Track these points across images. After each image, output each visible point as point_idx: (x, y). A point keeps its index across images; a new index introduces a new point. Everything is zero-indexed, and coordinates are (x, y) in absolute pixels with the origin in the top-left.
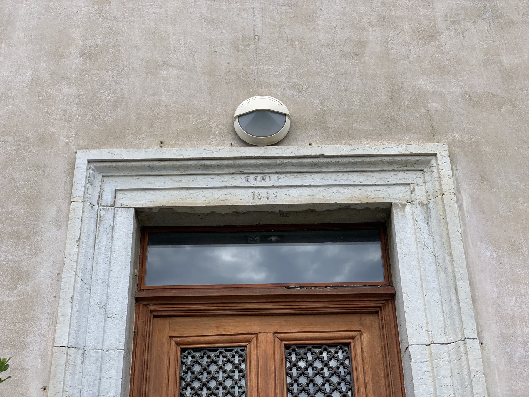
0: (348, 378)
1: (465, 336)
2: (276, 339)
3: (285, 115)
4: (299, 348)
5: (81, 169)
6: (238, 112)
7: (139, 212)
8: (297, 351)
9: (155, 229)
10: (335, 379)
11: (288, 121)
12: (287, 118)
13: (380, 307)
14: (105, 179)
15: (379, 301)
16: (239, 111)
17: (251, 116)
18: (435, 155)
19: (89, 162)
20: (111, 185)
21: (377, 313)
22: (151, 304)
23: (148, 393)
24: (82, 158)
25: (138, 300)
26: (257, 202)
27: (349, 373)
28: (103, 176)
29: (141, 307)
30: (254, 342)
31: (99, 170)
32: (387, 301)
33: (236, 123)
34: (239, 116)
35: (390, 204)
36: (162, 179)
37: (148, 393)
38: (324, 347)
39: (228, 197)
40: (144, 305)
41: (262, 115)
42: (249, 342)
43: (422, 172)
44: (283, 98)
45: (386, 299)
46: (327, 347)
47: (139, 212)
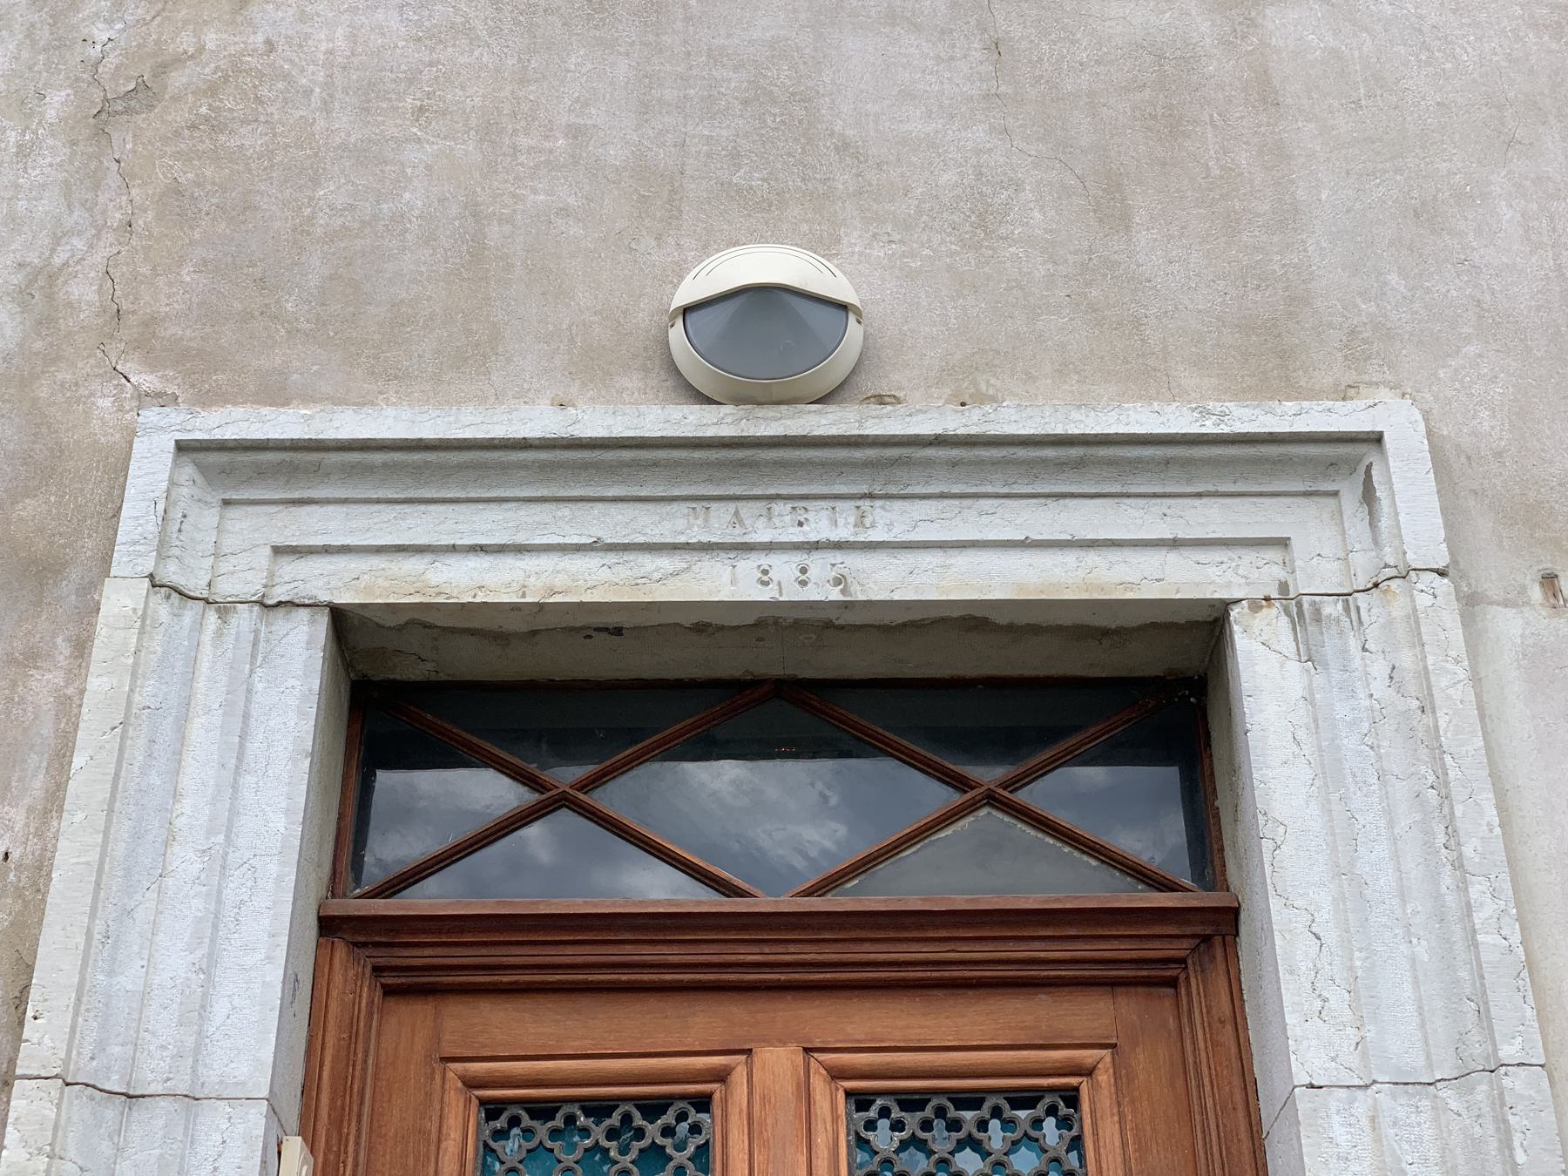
1: (1375, 1077)
3: (843, 307)
4: (1017, 1104)
5: (151, 465)
8: (952, 1113)
9: (401, 698)
11: (854, 331)
12: (852, 318)
13: (1183, 961)
15: (1182, 945)
16: (691, 290)
17: (731, 306)
18: (1377, 439)
19: (182, 448)
21: (1172, 983)
22: (381, 949)
23: (1111, 463)
25: (328, 926)
30: (739, 1077)
32: (1206, 939)
33: (677, 334)
34: (686, 311)
35: (1226, 605)
37: (1111, 463)
38: (1048, 1100)
40: (355, 944)
42: (1089, 1072)
43: (1331, 501)
45: (1198, 930)
46: (949, 1104)
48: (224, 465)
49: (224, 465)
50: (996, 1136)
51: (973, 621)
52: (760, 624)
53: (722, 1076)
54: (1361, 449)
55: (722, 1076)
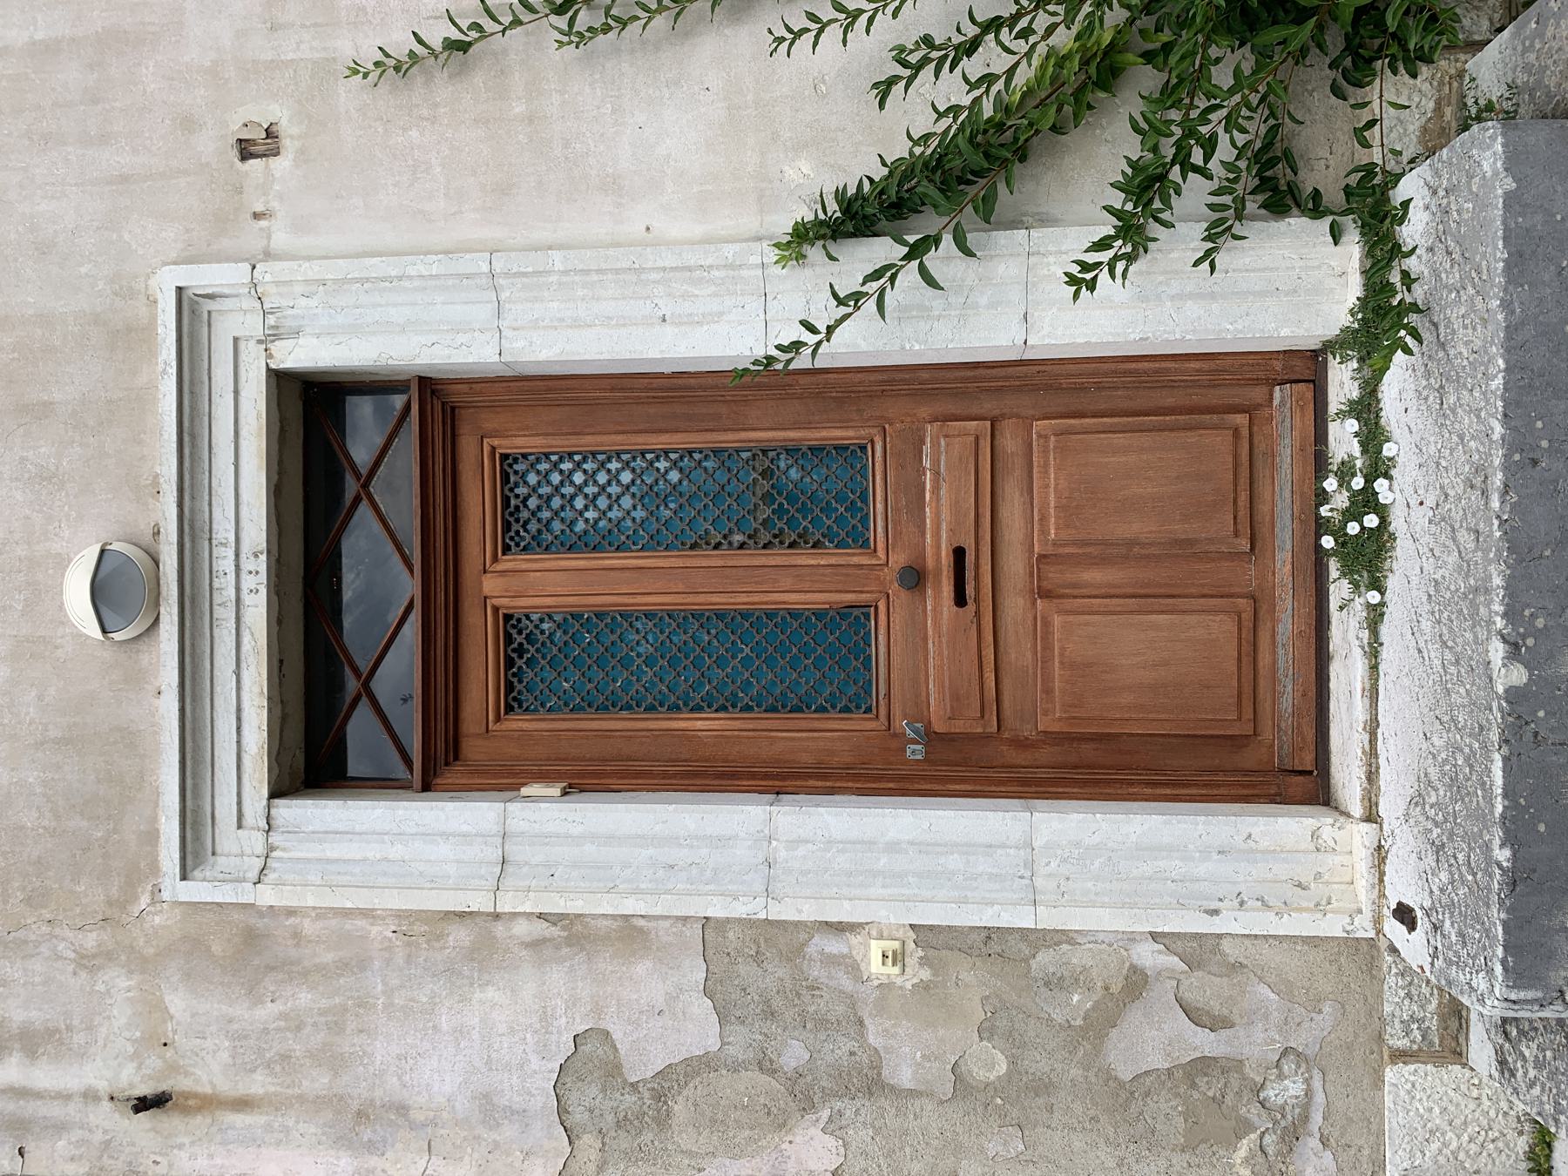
0: (577, 458)
2: (499, 567)
3: (103, 551)
4: (508, 481)
6: (96, 632)
7: (278, 791)
10: (602, 478)
14: (218, 850)
15: (436, 402)
17: (104, 610)
18: (180, 290)
19: (184, 878)
20: (227, 836)
21: (453, 409)
23: (192, 421)
24: (176, 890)
25: (426, 787)
26: (263, 591)
27: (618, 455)
28: (214, 854)
29: (439, 781)
30: (496, 602)
31: (199, 861)
32: (433, 392)
33: (117, 636)
34: (104, 631)
36: (219, 723)
39: (255, 723)
41: (106, 592)
44: (62, 563)
47: (278, 791)
48: (194, 851)
49: (194, 851)
50: (522, 491)
51: (276, 492)
52: (277, 594)
53: (493, 449)
54: (185, 298)
55: (496, 609)
